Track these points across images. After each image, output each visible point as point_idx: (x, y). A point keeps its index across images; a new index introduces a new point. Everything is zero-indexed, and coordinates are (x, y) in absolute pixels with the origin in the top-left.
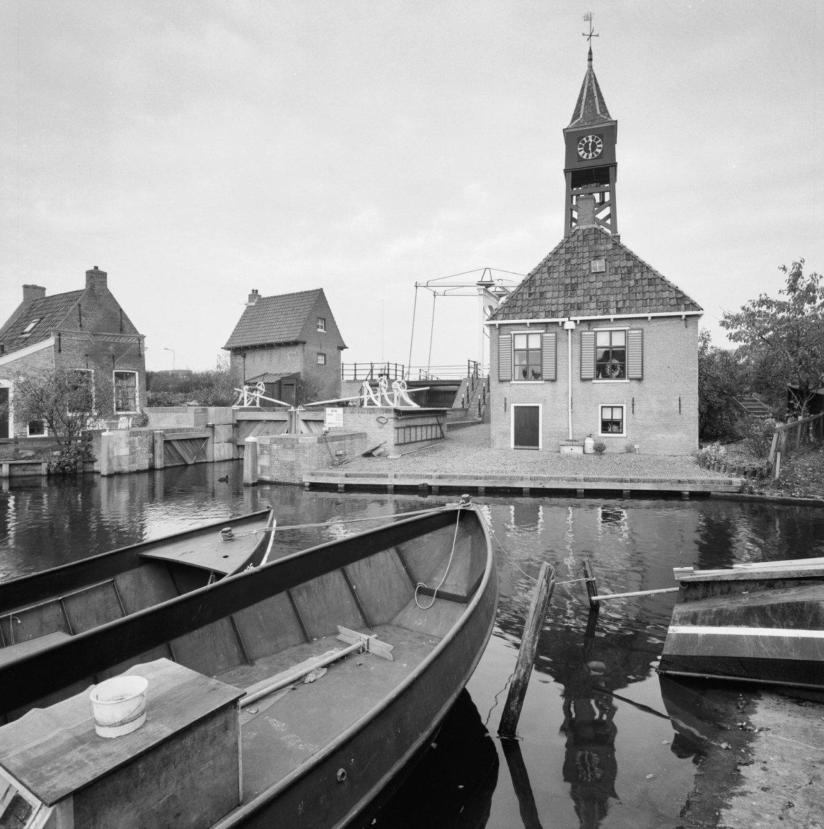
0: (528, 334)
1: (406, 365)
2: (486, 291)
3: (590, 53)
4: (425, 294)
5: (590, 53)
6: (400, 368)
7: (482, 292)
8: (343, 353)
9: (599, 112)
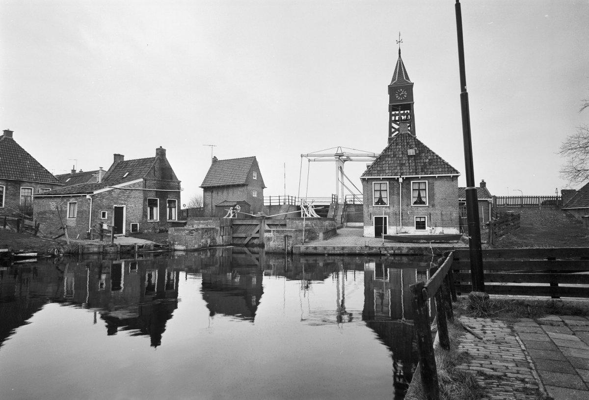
0: (381, 184)
1: (297, 197)
2: (339, 159)
3: (400, 50)
4: (305, 159)
5: (400, 50)
6: (294, 198)
7: (337, 159)
8: (264, 190)
9: (405, 79)
